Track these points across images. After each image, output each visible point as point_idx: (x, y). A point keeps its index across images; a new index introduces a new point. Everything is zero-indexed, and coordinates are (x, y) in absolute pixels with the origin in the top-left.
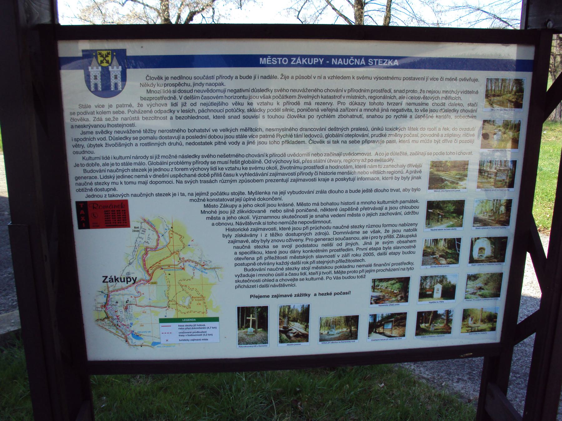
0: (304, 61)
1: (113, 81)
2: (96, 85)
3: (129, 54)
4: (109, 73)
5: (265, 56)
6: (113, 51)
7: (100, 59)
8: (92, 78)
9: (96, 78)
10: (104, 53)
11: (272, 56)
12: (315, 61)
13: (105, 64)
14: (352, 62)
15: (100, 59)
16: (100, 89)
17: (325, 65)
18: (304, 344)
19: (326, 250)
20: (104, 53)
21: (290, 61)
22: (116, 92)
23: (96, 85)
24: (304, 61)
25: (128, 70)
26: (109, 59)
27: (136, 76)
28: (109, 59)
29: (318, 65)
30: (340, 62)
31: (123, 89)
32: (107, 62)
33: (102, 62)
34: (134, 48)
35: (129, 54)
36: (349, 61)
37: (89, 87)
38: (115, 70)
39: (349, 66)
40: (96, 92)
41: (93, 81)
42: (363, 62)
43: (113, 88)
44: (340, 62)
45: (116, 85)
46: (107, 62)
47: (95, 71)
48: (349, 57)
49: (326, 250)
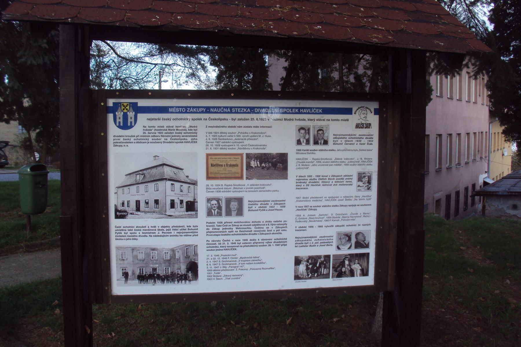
0: (194, 110)
1: (129, 120)
2: (119, 122)
3: (139, 105)
4: (127, 115)
5: (173, 107)
6: (130, 103)
7: (123, 108)
8: (118, 118)
9: (131, 118)
10: (125, 104)
11: (176, 107)
12: (201, 110)
13: (125, 111)
14: (222, 110)
15: (123, 108)
16: (122, 125)
17: (206, 112)
18: (276, 183)
19: (253, 188)
20: (125, 104)
21: (187, 110)
22: (131, 127)
23: (119, 122)
24: (194, 110)
25: (138, 114)
26: (128, 108)
27: (142, 117)
28: (128, 108)
29: (203, 112)
30: (215, 110)
31: (135, 124)
32: (127, 109)
33: (124, 109)
34: (142, 103)
35: (139, 105)
36: (220, 110)
37: (116, 124)
38: (131, 114)
39: (220, 113)
40: (119, 127)
41: (118, 121)
42: (229, 110)
43: (129, 125)
44: (215, 110)
45: (131, 122)
46: (127, 109)
47: (120, 114)
48: (220, 107)
49: (253, 188)
